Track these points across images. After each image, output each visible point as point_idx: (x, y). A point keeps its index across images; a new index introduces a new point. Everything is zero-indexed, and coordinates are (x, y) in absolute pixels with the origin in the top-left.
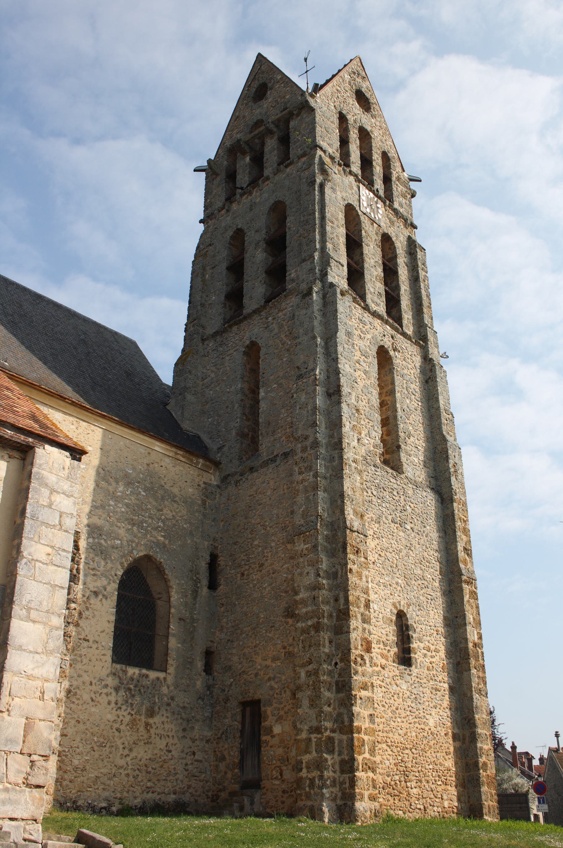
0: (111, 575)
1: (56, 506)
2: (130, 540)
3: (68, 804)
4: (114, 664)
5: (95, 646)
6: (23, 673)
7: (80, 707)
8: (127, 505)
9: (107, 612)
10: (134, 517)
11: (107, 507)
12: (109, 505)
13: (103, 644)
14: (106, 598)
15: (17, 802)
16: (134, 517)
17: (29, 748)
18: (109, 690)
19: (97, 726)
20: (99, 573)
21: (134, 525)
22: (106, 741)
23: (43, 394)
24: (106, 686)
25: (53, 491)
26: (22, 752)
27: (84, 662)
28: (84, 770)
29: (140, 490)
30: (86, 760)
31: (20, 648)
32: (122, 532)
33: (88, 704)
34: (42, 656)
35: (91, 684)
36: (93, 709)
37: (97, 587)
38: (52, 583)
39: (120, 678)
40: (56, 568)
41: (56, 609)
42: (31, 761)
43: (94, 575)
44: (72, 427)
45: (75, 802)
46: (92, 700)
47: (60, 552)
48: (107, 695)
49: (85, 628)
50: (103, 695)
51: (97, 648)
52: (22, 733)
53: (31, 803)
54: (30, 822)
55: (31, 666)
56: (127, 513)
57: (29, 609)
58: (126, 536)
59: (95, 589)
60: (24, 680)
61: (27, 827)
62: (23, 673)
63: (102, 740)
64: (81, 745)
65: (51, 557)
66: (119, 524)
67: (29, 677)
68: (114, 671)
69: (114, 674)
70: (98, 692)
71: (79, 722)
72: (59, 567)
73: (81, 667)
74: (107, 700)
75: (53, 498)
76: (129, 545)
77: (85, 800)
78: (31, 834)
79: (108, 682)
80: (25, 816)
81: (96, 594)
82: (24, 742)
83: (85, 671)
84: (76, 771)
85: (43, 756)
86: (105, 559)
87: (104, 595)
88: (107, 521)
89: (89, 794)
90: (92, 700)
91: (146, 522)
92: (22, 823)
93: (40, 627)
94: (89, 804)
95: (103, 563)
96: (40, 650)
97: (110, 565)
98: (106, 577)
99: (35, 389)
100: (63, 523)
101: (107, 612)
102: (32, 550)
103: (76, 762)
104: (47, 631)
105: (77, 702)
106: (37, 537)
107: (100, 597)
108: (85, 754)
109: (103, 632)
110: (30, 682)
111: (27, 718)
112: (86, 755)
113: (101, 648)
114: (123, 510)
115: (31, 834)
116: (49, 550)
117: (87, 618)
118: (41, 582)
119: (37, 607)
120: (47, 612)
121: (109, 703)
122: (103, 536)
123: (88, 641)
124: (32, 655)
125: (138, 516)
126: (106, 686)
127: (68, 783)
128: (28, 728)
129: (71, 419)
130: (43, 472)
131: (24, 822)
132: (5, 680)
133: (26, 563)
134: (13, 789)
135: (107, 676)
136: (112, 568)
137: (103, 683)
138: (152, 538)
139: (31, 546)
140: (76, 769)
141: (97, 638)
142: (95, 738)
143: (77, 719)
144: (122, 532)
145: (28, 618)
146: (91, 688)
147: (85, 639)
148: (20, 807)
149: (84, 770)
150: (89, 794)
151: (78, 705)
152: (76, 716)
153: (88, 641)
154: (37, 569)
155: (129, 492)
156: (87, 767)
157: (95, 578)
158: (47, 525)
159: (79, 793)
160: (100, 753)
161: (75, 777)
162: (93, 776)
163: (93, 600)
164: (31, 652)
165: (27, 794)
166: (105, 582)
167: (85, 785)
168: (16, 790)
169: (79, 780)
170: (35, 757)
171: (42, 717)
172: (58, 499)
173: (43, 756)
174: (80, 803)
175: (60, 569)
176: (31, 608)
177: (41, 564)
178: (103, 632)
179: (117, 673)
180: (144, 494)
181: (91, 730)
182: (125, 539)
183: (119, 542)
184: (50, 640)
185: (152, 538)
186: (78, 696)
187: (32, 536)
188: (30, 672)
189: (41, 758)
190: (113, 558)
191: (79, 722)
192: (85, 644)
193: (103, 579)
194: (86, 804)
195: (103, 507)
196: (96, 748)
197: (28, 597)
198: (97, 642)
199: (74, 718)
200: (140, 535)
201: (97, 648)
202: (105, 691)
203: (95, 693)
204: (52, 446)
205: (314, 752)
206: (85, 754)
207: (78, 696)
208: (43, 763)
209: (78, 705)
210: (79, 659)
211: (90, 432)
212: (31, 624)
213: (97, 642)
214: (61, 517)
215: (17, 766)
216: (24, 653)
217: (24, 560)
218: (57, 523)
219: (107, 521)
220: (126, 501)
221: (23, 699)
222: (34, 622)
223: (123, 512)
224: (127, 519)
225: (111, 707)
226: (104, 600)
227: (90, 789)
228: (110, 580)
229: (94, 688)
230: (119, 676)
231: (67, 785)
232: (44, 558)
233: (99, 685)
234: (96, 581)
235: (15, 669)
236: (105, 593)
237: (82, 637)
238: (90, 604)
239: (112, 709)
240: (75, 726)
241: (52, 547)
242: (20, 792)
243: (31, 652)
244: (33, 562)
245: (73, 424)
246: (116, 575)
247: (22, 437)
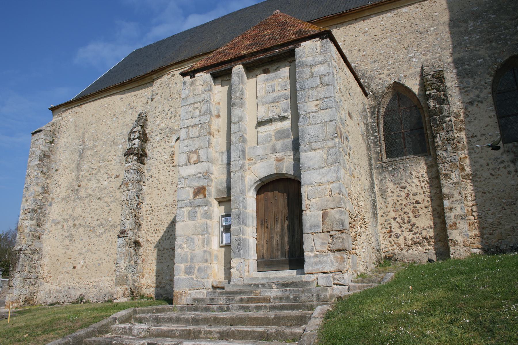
0: (482, 85)
1: (316, 74)
2: (491, 54)
3: (492, 250)
4: (505, 145)
5: (483, 138)
6: (314, 183)
7: (483, 182)
8: (481, 32)
9: (486, 111)
10: (490, 37)
11: (463, 43)
12: (465, 40)
13: (490, 134)
14: (482, 102)
15: (325, 262)
16: (490, 37)
17: (327, 228)
18: (506, 164)
19: (503, 192)
20: (470, 88)
21: (492, 42)
22: (514, 201)
23: (388, 5)
24: (503, 162)
25: (312, 66)
26: (324, 231)
27: (477, 151)
28: (500, 224)
29: (489, 16)
30: (500, 217)
31: (309, 169)
32: (482, 52)
33: (489, 178)
34: (325, 168)
35: (488, 164)
36: (495, 181)
37: (471, 98)
38: (323, 121)
39: (514, 153)
40: (324, 111)
41: (330, 136)
42: (330, 236)
43: (466, 92)
44: (417, 10)
45: (497, 248)
46: (492, 175)
47: (325, 100)
48: (505, 167)
49: (471, 129)
50: (501, 169)
51: (486, 139)
52: (321, 220)
53: (335, 261)
54: (338, 273)
55: (319, 178)
56: (482, 37)
57: (310, 144)
58: (486, 53)
59: (470, 100)
60: (316, 187)
61: (335, 277)
62: (314, 183)
63: (510, 200)
64: (491, 208)
65: (319, 106)
66: (478, 48)
67: (319, 184)
68: (506, 149)
69: (508, 151)
70: (496, 168)
71: (485, 193)
72: (326, 109)
73: (475, 156)
74: (507, 172)
75: (313, 71)
76: (491, 58)
77: (507, 245)
78: (339, 281)
79: (503, 159)
80: (332, 270)
81: (471, 103)
82: (323, 225)
83: (480, 158)
84: (492, 227)
85: (338, 231)
86: (472, 77)
87: (478, 102)
88: (466, 51)
89: (509, 240)
90: (492, 175)
91: (502, 34)
92: (331, 275)
93: (320, 151)
94: (512, 247)
95: (471, 80)
96: (323, 165)
97: (478, 79)
98: (476, 88)
99: (381, 5)
100: (323, 81)
101: (486, 111)
102: (305, 108)
103: (491, 220)
104: (326, 152)
105: (479, 180)
106: (307, 99)
107: (476, 103)
108: (497, 213)
109: (488, 125)
110: (320, 187)
111: (323, 210)
112: (499, 214)
113: (489, 137)
114: (478, 37)
115: (339, 281)
116: (317, 102)
117: (470, 122)
118: (315, 124)
119: (316, 140)
120: (324, 140)
121: (509, 173)
122: (466, 63)
123: (476, 136)
124: (317, 171)
125: (494, 34)
126: (503, 162)
127: (489, 236)
128: (325, 215)
129: (415, 6)
130: (303, 59)
131: (333, 274)
132: (302, 191)
133: (303, 118)
134: (321, 255)
135: (501, 155)
136: (481, 80)
137: (499, 161)
138: (513, 43)
139: (304, 106)
140: (492, 225)
141: (483, 132)
142: (504, 201)
143: (483, 191)
144: (482, 52)
145: (311, 149)
146: (488, 167)
147: (473, 137)
148: (327, 265)
149: (500, 224)
150: (509, 240)
151: (480, 181)
152: (481, 190)
153: (476, 136)
154: (311, 118)
155: (479, 23)
156: (502, 222)
157: (467, 93)
158: (312, 88)
159: (500, 241)
160: (511, 210)
161: (494, 231)
162: (509, 227)
163: (470, 109)
164: (317, 169)
165: (332, 256)
166: (477, 92)
167: (503, 235)
168: (323, 255)
169: (497, 232)
170: (332, 233)
171: (332, 206)
172: (315, 69)
173: (338, 231)
174: (502, 247)
175: (327, 110)
176: (312, 143)
177: (313, 114)
178: (488, 125)
179: (510, 150)
180: (494, 16)
181: (498, 196)
182: (487, 55)
183: (482, 60)
184: (329, 157)
185: (513, 43)
186: (478, 176)
187: (304, 100)
188: (318, 181)
189: (337, 232)
190: (479, 73)
191: (485, 193)
192: (475, 139)
193: (474, 90)
194: (508, 247)
195: (459, 44)
196: (506, 207)
197: (308, 137)
198: (484, 135)
199: (480, 191)
200: (500, 46)
201: (486, 139)
202: (502, 165)
203: (493, 170)
204: (305, 41)
205: (185, 212)
206: (497, 213)
207: (478, 176)
208: (340, 235)
209: (480, 181)
210: (473, 151)
211: (433, 4)
212: (314, 152)
213: (484, 135)
214: (320, 78)
215: (321, 241)
216: (312, 171)
217: (302, 116)
218: (319, 83)
219: (466, 51)
220: (479, 30)
221: (318, 199)
222: (315, 150)
223: (478, 39)
224: (483, 42)
225: (511, 175)
226: (480, 105)
227: (510, 237)
228: (481, 89)
229: (491, 166)
230: (512, 151)
231: (487, 237)
232: (314, 109)
233: (495, 163)
234: (468, 95)
235: (308, 183)
236: (480, 99)
237: (470, 136)
238: (469, 112)
239: (514, 176)
240: (482, 197)
241: (318, 100)
242: (326, 256)
243: (317, 169)
244: (308, 115)
245: (417, 8)
246: (486, 83)
247: (286, 48)
